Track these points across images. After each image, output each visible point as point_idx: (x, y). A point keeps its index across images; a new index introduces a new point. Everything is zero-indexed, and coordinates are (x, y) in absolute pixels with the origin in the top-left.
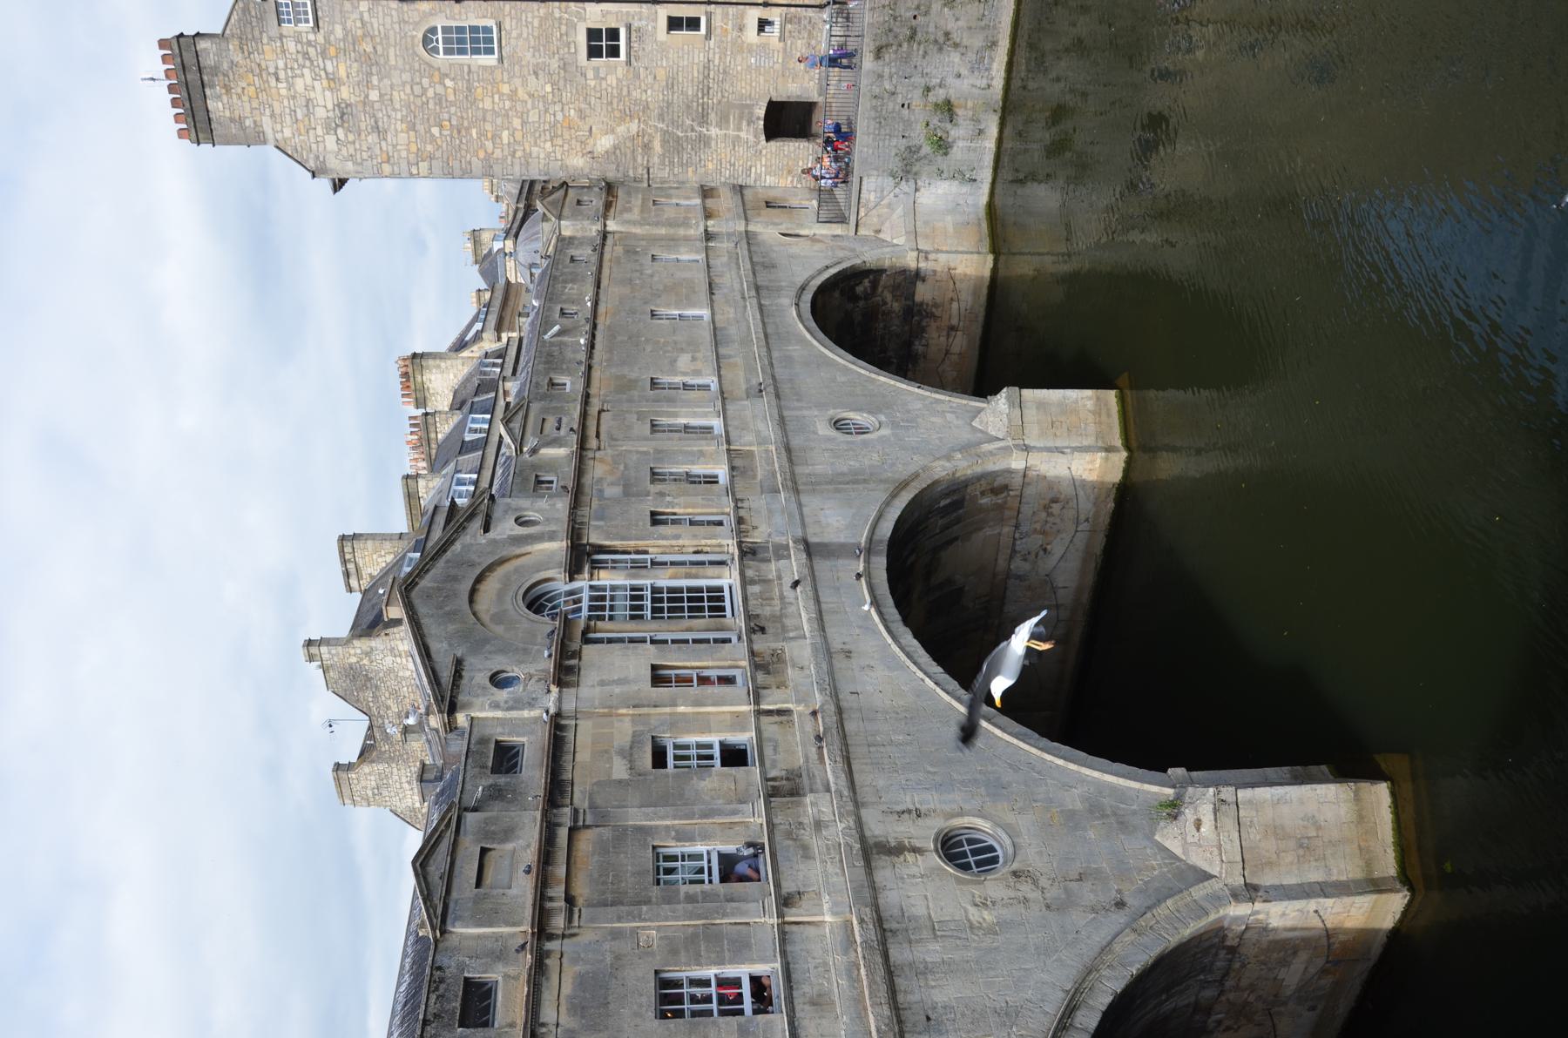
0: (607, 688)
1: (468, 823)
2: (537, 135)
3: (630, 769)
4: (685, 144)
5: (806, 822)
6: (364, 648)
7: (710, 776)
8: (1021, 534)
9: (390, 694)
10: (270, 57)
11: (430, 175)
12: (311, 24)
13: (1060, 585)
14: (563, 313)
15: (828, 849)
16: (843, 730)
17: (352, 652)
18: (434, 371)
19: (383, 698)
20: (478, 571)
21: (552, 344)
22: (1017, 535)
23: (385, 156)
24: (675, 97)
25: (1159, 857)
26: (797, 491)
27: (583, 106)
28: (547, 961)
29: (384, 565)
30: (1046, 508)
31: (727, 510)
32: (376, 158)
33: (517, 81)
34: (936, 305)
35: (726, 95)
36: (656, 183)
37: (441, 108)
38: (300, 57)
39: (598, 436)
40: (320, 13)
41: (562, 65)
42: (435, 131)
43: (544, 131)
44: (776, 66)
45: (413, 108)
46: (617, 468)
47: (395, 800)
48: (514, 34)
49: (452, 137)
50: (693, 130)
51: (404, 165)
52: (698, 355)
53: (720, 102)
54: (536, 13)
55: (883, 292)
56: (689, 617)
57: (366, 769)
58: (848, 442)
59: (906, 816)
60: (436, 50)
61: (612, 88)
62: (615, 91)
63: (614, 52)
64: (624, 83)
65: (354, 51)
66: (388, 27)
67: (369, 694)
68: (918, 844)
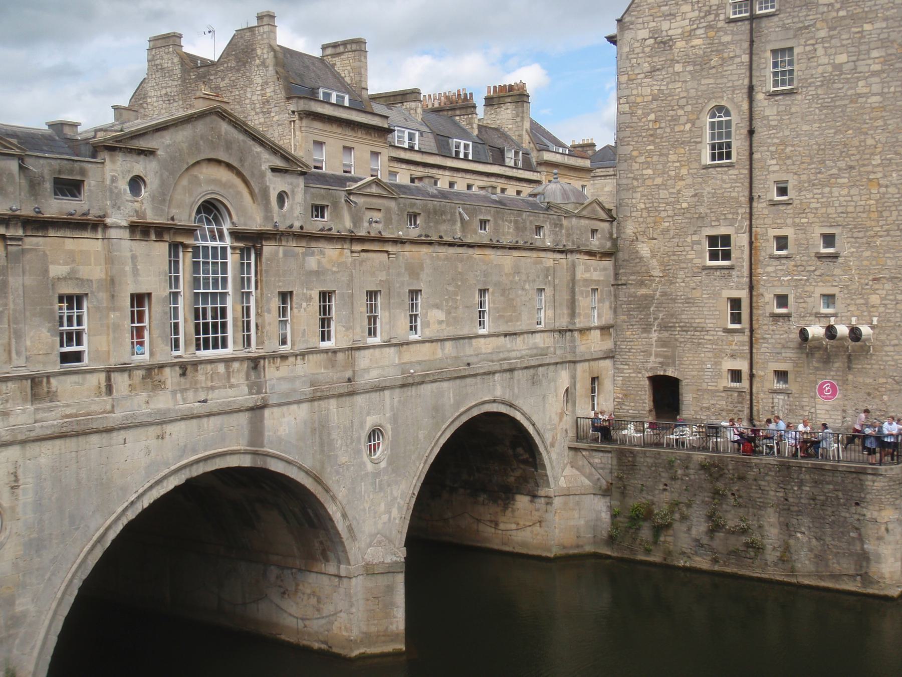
2: (650, 197)
3: (58, 278)
4: (644, 313)
5: (9, 405)
7: (52, 335)
9: (233, 81)
11: (620, 113)
12: (732, 17)
19: (230, 75)
20: (235, 164)
21: (453, 214)
22: (294, 570)
23: (633, 77)
24: (679, 305)
26: (312, 400)
27: (672, 232)
29: (343, 75)
30: (313, 593)
31: (296, 348)
32: (631, 70)
33: (689, 181)
34: (513, 511)
35: (682, 345)
36: (615, 291)
37: (670, 121)
38: (707, 8)
39: (363, 251)
40: (740, 23)
41: (702, 215)
42: (652, 117)
43: (653, 203)
45: (669, 98)
46: (333, 266)
47: (152, 83)
48: (725, 177)
49: (649, 129)
51: (627, 92)
53: (676, 340)
54: (741, 194)
55: (521, 468)
57: (176, 60)
59: (13, 478)
60: (713, 116)
61: (685, 256)
62: (683, 257)
63: (714, 256)
65: (712, 51)
67: (233, 64)
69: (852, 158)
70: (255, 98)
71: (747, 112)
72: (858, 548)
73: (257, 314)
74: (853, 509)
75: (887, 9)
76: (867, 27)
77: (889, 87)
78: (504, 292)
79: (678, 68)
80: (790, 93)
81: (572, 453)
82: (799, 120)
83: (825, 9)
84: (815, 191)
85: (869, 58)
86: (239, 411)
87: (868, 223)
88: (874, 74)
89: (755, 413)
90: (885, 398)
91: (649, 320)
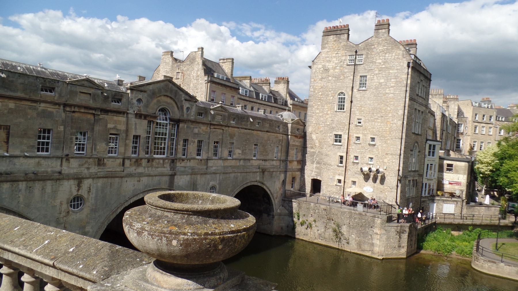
0: (134, 125)
6: (200, 63)
7: (106, 146)
10: (342, 52)
12: (349, 64)
15: (81, 170)
16: (115, 177)
17: (199, 60)
20: (173, 97)
28: (57, 106)
33: (330, 116)
40: (351, 66)
42: (320, 93)
44: (329, 183)
48: (342, 116)
49: (319, 98)
50: (315, 160)
51: (313, 85)
53: (322, 168)
57: (171, 59)
63: (336, 141)
68: (80, 191)
69: (383, 113)
70: (194, 74)
72: (371, 242)
73: (176, 145)
74: (370, 229)
75: (397, 66)
76: (391, 71)
77: (396, 92)
78: (263, 146)
79: (330, 78)
80: (365, 90)
82: (367, 99)
83: (378, 64)
84: (370, 123)
85: (391, 82)
86: (167, 176)
87: (386, 135)
88: (392, 87)
89: (344, 194)
90: (386, 193)
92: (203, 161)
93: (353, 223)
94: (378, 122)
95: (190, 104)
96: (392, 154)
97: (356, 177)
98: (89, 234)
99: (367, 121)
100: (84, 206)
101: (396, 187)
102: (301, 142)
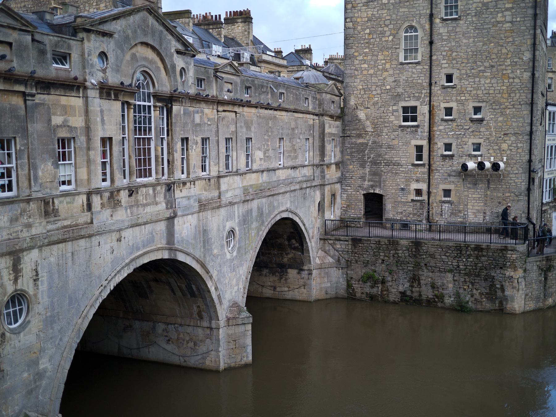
0: (99, 114)
1: (25, 36)
2: (365, 82)
3: (57, 126)
4: (361, 154)
7: (54, 168)
8: (177, 327)
13: (150, 350)
14: (281, 94)
15: (16, 232)
18: (243, 28)
20: (157, 47)
22: (176, 325)
24: (384, 149)
25: (12, 413)
31: (191, 176)
33: (391, 72)
34: (286, 280)
35: (386, 174)
37: (379, 34)
42: (368, 31)
43: (368, 85)
45: (379, 20)
46: (208, 121)
48: (414, 70)
50: (368, 158)
52: (263, 161)
53: (382, 171)
54: (424, 81)
56: (136, 159)
58: (223, 237)
59: (35, 274)
60: (406, 32)
62: (387, 120)
63: (405, 119)
64: (391, 124)
66: (418, 8)
68: (20, 281)
71: (428, 30)
73: (169, 153)
74: (498, 271)
77: (516, 18)
80: (455, 19)
81: (322, 242)
82: (461, 36)
84: (470, 80)
87: (502, 100)
88: (507, 9)
91: (365, 159)
92: (212, 181)
93: (465, 265)
94: (486, 77)
95: (185, 62)
96: (515, 134)
97: (450, 183)
98: (47, 374)
99: (465, 76)
100: (30, 314)
101: (526, 192)
102: (337, 127)
